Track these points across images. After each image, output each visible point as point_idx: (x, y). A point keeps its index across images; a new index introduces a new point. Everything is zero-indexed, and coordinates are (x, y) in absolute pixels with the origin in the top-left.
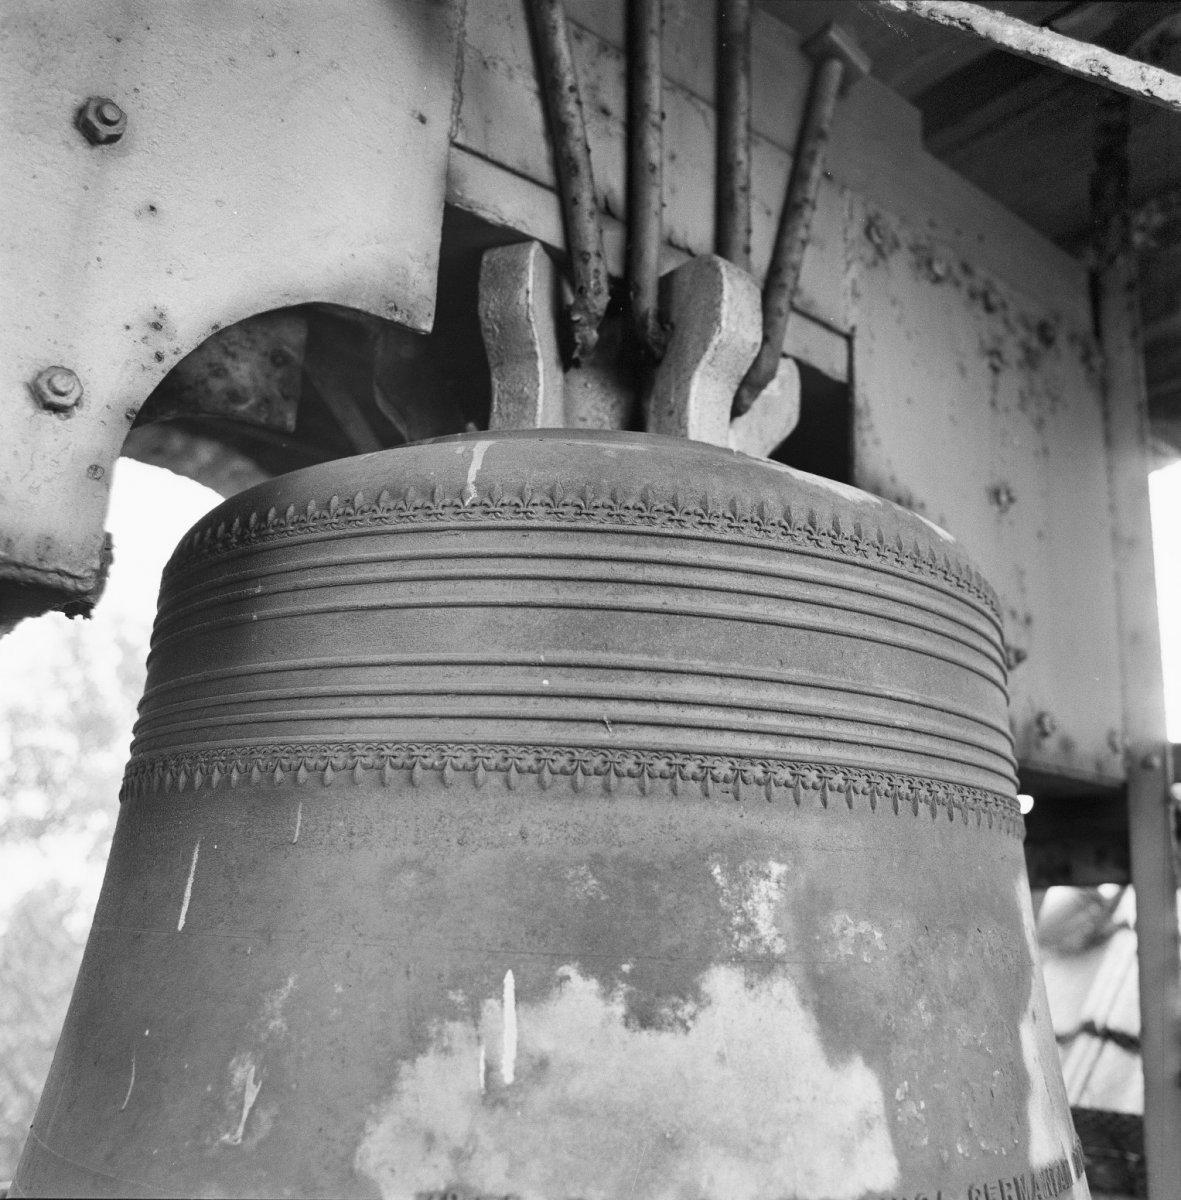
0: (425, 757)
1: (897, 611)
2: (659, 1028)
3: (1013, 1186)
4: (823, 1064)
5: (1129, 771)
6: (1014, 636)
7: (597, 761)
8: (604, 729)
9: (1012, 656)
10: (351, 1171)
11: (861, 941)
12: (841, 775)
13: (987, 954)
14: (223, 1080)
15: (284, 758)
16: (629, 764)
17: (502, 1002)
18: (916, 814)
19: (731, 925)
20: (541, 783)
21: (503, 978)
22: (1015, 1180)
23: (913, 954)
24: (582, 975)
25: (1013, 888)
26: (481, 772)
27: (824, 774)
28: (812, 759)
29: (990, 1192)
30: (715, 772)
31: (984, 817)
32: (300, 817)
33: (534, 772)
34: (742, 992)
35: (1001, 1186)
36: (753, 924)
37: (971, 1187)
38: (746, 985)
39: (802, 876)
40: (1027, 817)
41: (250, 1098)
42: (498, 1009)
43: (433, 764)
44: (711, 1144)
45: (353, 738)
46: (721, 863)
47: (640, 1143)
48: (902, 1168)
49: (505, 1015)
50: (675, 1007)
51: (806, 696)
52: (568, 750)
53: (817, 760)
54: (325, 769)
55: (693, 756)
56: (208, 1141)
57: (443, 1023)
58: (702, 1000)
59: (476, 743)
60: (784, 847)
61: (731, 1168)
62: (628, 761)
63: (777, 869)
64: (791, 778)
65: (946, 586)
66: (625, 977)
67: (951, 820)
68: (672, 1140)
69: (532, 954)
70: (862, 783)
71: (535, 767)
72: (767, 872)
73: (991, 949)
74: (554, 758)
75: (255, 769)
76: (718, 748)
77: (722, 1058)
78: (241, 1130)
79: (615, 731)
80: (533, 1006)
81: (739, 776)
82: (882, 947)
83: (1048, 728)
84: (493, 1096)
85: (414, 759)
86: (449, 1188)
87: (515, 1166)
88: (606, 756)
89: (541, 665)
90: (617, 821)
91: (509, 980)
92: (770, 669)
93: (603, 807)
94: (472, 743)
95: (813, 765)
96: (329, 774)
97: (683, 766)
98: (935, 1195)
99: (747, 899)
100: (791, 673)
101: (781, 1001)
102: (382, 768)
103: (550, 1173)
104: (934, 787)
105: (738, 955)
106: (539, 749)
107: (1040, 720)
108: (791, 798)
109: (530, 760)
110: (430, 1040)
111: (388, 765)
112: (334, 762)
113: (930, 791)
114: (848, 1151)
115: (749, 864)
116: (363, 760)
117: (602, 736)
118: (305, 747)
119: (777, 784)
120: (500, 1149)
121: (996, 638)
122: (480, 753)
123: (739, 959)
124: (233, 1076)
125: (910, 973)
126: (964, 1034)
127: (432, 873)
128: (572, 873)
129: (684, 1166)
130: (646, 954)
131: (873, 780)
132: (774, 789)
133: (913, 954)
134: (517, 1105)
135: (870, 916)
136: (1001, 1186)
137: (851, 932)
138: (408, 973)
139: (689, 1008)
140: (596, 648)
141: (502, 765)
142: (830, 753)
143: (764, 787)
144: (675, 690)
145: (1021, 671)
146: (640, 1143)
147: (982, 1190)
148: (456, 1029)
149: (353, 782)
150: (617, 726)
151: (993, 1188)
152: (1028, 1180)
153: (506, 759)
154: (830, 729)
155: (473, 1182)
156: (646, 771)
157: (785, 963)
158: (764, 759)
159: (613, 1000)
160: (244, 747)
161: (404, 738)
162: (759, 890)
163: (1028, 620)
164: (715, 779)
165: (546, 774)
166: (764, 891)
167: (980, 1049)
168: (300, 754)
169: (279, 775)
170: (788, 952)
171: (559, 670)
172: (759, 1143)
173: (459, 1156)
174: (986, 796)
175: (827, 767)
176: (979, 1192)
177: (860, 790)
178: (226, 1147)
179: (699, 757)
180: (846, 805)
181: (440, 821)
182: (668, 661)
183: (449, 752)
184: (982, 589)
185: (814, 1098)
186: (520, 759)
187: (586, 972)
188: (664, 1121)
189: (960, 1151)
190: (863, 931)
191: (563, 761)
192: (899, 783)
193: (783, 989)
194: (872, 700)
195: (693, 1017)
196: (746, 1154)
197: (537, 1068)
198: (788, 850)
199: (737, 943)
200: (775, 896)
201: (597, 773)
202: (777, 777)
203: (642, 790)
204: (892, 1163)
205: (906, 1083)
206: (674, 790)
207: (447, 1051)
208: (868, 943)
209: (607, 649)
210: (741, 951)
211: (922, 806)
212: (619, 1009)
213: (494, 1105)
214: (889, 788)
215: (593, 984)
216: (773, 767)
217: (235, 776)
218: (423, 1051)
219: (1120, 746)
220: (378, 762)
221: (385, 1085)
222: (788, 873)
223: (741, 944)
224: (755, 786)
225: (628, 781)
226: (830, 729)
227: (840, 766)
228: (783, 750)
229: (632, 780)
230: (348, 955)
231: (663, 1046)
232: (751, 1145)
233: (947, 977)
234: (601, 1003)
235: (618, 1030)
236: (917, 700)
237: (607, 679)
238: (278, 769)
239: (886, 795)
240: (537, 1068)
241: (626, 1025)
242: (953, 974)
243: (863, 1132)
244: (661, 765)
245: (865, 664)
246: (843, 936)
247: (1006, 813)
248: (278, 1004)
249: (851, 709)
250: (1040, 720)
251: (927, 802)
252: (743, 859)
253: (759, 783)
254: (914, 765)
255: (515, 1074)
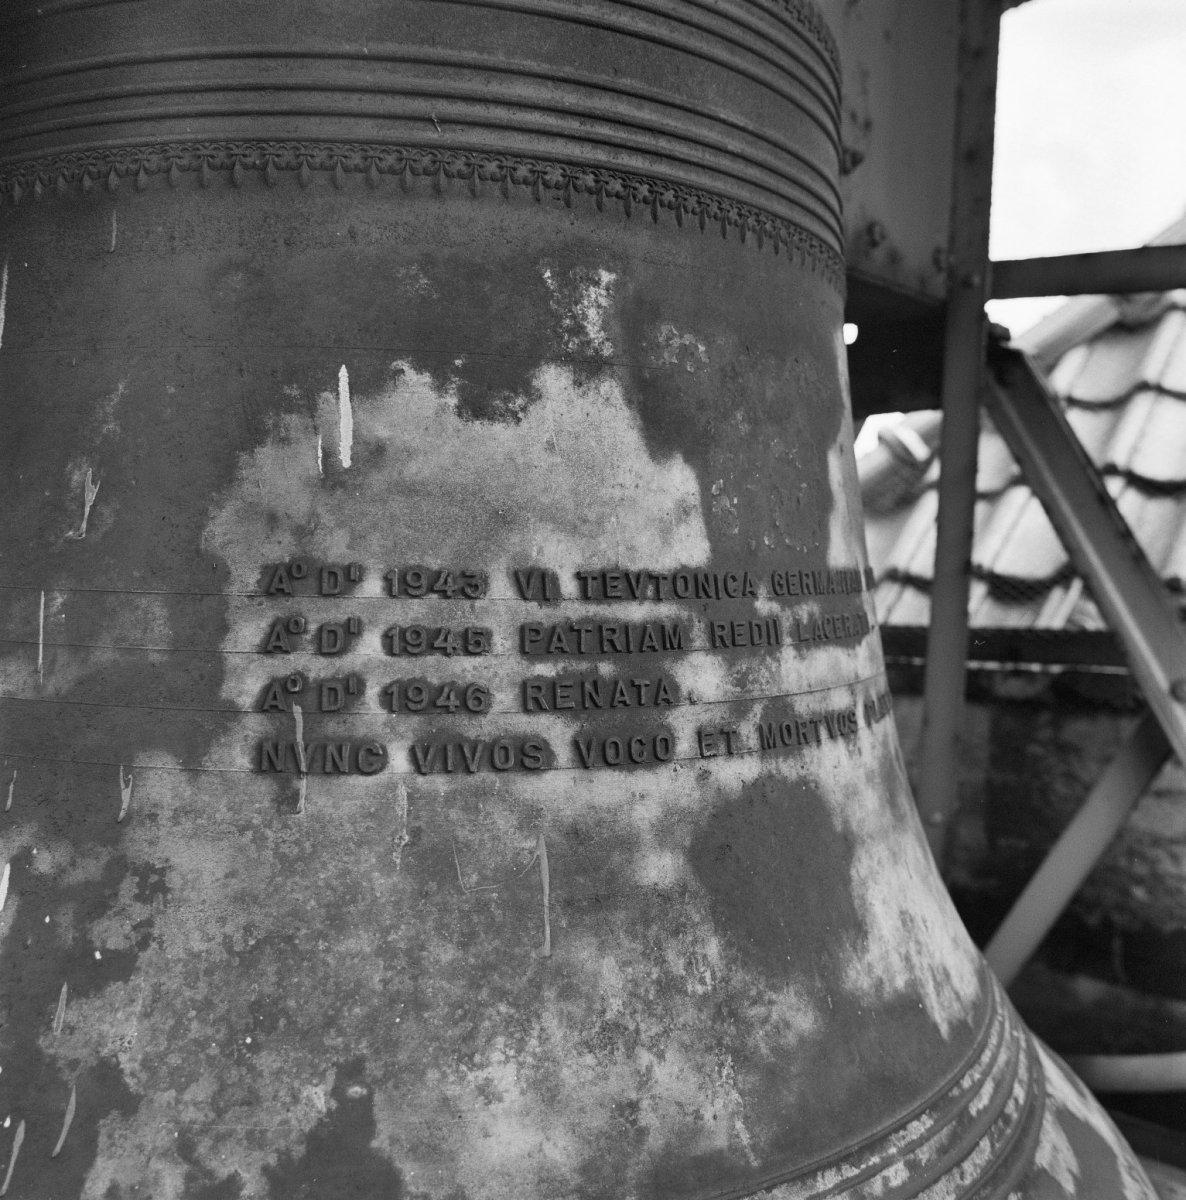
0: (245, 156)
1: (736, 32)
2: (492, 419)
3: (811, 577)
4: (645, 457)
5: (950, 291)
6: (850, 136)
7: (426, 160)
8: (433, 128)
9: (848, 158)
10: (198, 551)
11: (686, 352)
12: (672, 192)
13: (802, 383)
14: (62, 484)
15: (92, 164)
16: (459, 165)
17: (338, 394)
18: (743, 240)
19: (561, 327)
20: (368, 182)
21: (338, 372)
22: (813, 573)
23: (733, 369)
24: (415, 369)
25: (832, 334)
26: (305, 171)
27: (656, 189)
28: (644, 173)
29: (790, 579)
30: (547, 177)
31: (809, 259)
32: (115, 225)
33: (361, 171)
34: (571, 389)
35: (801, 576)
36: (583, 328)
37: (774, 572)
38: (575, 382)
39: (631, 286)
40: (850, 348)
41: (90, 497)
42: (334, 401)
43: (254, 163)
44: (541, 520)
45: (166, 138)
46: (552, 268)
47: (474, 518)
48: (713, 550)
49: (343, 412)
50: (507, 400)
51: (640, 108)
52: (395, 148)
53: (648, 174)
54: (137, 173)
55: (524, 160)
56: (52, 538)
57: (278, 415)
58: (534, 395)
59: (298, 141)
60: (614, 256)
61: (559, 541)
62: (459, 162)
63: (606, 277)
64: (622, 189)
65: (786, 16)
66: (457, 371)
67: (777, 253)
68: (504, 517)
69: (365, 349)
70: (692, 202)
71: (362, 166)
72: (597, 278)
73: (806, 379)
74: (382, 156)
75: (61, 179)
76: (550, 153)
77: (550, 447)
78: (84, 525)
79: (444, 131)
80: (368, 398)
81: (570, 182)
82: (705, 359)
83: (877, 237)
84: (332, 478)
85: (234, 158)
86: (293, 560)
87: (356, 540)
88: (436, 156)
89: (364, 58)
90: (447, 222)
91: (343, 373)
92: (604, 76)
93: (434, 208)
94: (294, 140)
95: (645, 179)
96: (142, 177)
97: (515, 169)
98: (743, 574)
99: (576, 305)
100: (625, 82)
101: (608, 399)
102: (199, 169)
103: (389, 544)
104: (763, 218)
105: (568, 355)
106: (365, 147)
107: (870, 228)
108: (622, 209)
109: (356, 159)
110: (267, 433)
111: (205, 165)
112: (147, 165)
113: (758, 221)
114: (665, 532)
115: (580, 270)
116: (178, 161)
117: (431, 135)
118: (114, 151)
119: (609, 195)
120: (340, 525)
121: (834, 93)
122: (303, 151)
123: (564, 359)
124: (70, 480)
125: (729, 386)
126: (777, 446)
127: (259, 274)
128: (403, 271)
129: (515, 539)
130: (477, 350)
131: (702, 200)
132: (605, 199)
133: (733, 369)
134: (356, 487)
135: (696, 332)
136: (801, 576)
137: (676, 342)
138: (241, 370)
139: (520, 401)
140: (422, 42)
141: (328, 163)
142: (663, 169)
143: (595, 196)
144: (504, 91)
145: (857, 174)
146: (474, 518)
147: (784, 575)
148: (293, 420)
149: (170, 185)
150: (446, 126)
151: (793, 576)
152: (824, 576)
153: (331, 157)
154: (663, 144)
155: (317, 554)
156: (476, 172)
157: (612, 365)
158: (596, 168)
159: (446, 393)
160: (44, 157)
161: (221, 136)
162: (589, 296)
163: (868, 125)
164: (546, 185)
165: (374, 172)
166: (593, 296)
167: (790, 462)
168: (108, 159)
169: (87, 182)
170: (615, 356)
171: (384, 64)
172: (585, 521)
173: (302, 532)
174: (811, 239)
175: (658, 182)
176: (780, 576)
177: (690, 209)
178: (70, 541)
179: (529, 161)
180: (675, 222)
181: (265, 221)
182: (499, 59)
183: (271, 150)
184: (820, 30)
185: (637, 486)
186: (346, 157)
187: (419, 368)
188: (497, 500)
189: (767, 542)
190: (687, 343)
191: (390, 160)
192: (728, 207)
193: (610, 387)
194: (706, 121)
195: (524, 409)
196: (574, 530)
197: (372, 453)
198: (618, 260)
199: (567, 344)
200: (603, 302)
201: (426, 172)
202: (609, 188)
203: (473, 191)
204: (706, 545)
205: (721, 481)
206: (505, 193)
207: (285, 441)
208: (692, 354)
209: (434, 44)
210: (571, 351)
211: (749, 235)
212: (452, 401)
213: (333, 488)
214: (718, 211)
215: (427, 378)
216: (605, 176)
217: (38, 189)
218: (261, 443)
219: (944, 265)
220: (195, 163)
221: (226, 475)
222: (616, 281)
223: (570, 346)
224: (586, 195)
225: (456, 181)
226: (663, 144)
227: (672, 182)
228: (614, 161)
229: (462, 181)
230: (179, 357)
231: (501, 434)
232: (578, 523)
233: (764, 394)
234: (433, 395)
235: (453, 420)
236: (751, 128)
237: (435, 76)
238: (86, 177)
239: (715, 217)
240: (372, 453)
241: (460, 415)
242: (769, 394)
243: (680, 519)
244: (492, 167)
245: (701, 83)
246: (669, 345)
247: (830, 262)
248: (109, 409)
249: (685, 127)
250: (870, 228)
251: (754, 231)
252: (572, 266)
253: (590, 191)
254: (744, 193)
255: (352, 459)
